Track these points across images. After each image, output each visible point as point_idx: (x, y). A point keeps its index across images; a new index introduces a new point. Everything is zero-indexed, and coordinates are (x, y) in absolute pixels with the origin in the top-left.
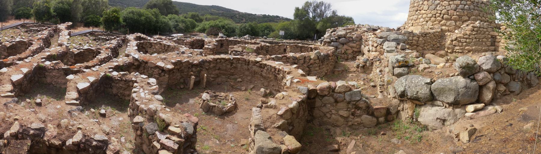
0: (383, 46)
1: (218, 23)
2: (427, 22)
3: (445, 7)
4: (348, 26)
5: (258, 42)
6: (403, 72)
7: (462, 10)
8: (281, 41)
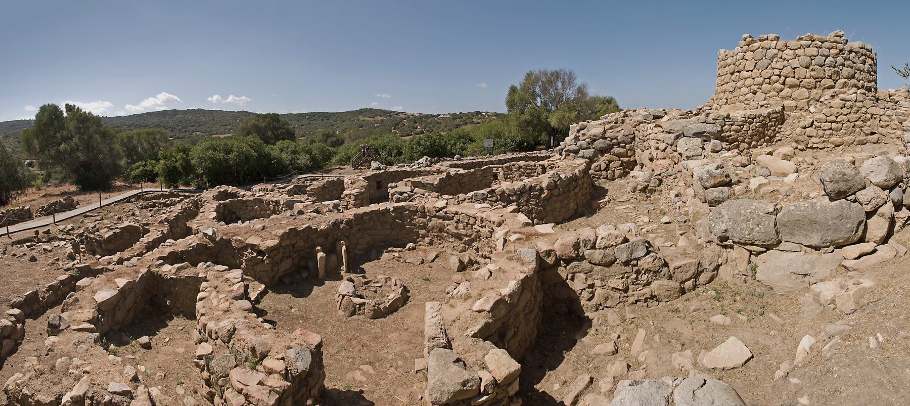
0: (676, 146)
1: (372, 142)
2: (755, 93)
3: (788, 61)
4: (607, 115)
5: (443, 168)
6: (721, 196)
7: (822, 67)
8: (487, 160)
